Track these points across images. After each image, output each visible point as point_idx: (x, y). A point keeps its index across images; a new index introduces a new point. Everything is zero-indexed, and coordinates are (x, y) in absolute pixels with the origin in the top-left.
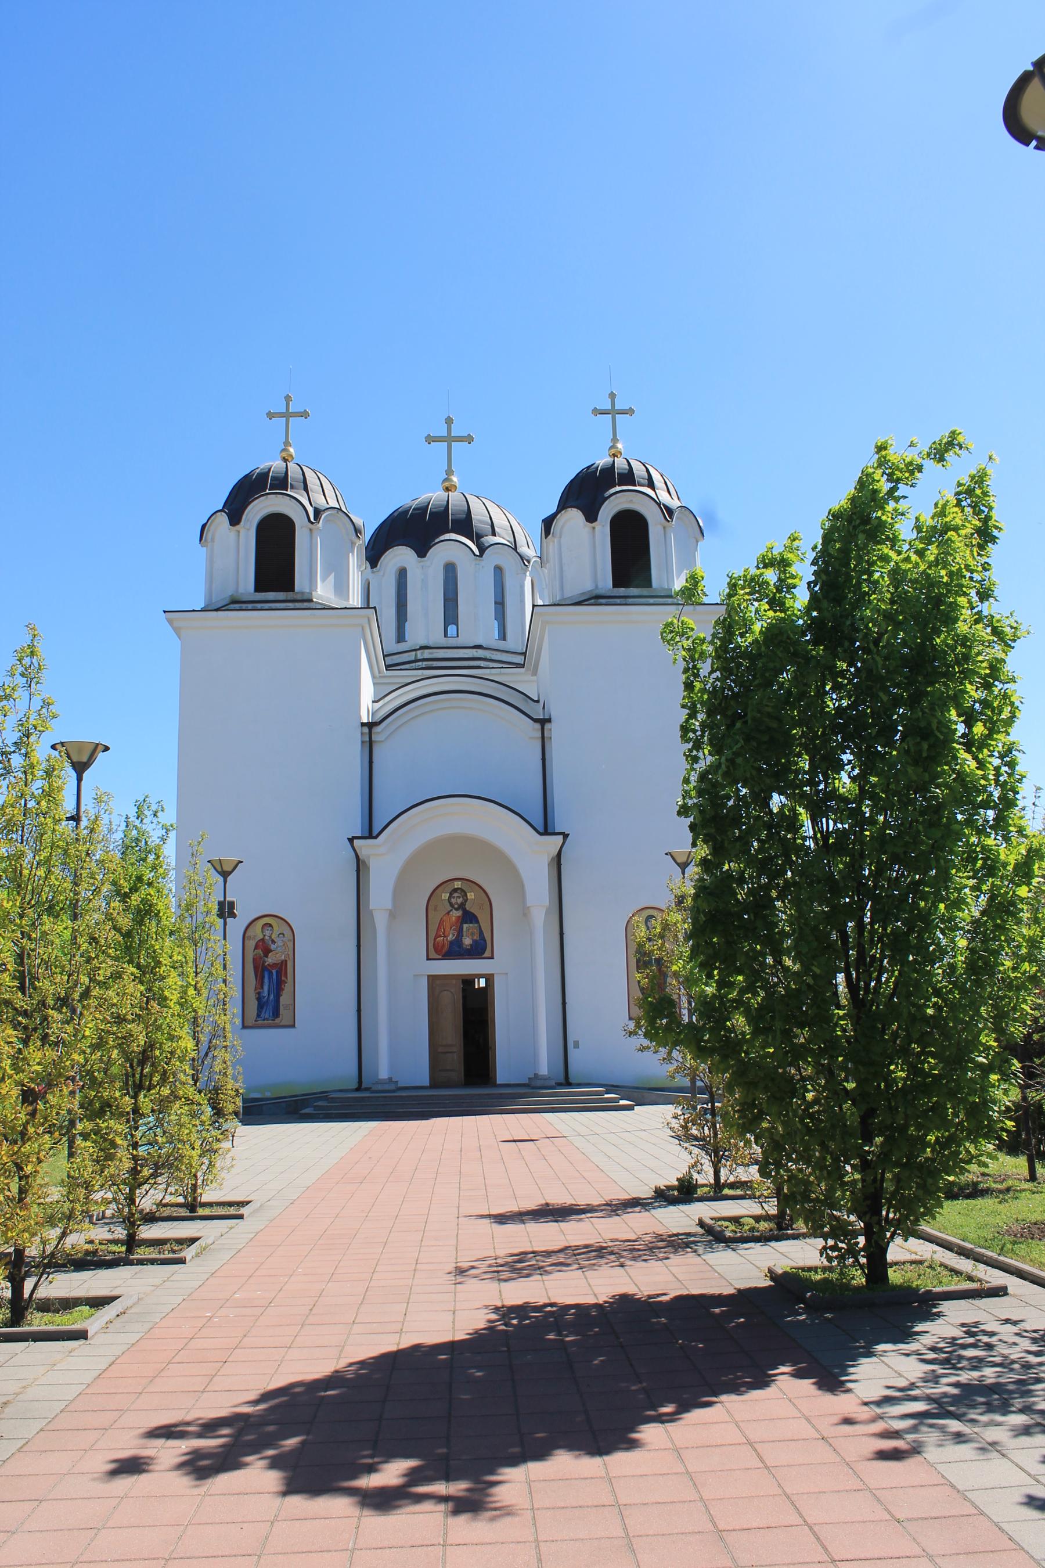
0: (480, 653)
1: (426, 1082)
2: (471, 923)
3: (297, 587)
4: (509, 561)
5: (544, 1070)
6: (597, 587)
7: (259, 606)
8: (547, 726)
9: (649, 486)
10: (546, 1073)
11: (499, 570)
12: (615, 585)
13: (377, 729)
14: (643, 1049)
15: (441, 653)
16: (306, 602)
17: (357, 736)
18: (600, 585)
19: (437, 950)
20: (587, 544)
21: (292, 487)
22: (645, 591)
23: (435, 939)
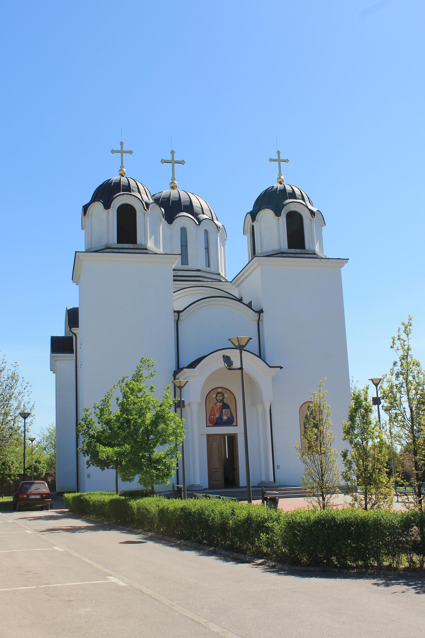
1: (207, 486)
2: (227, 409)
3: (138, 241)
4: (211, 229)
5: (198, 482)
6: (280, 248)
7: (121, 251)
8: (261, 314)
9: (302, 200)
10: (264, 480)
11: (206, 231)
13: (181, 314)
16: (144, 250)
17: (172, 318)
18: (282, 247)
20: (273, 228)
21: (133, 191)
23: (210, 417)
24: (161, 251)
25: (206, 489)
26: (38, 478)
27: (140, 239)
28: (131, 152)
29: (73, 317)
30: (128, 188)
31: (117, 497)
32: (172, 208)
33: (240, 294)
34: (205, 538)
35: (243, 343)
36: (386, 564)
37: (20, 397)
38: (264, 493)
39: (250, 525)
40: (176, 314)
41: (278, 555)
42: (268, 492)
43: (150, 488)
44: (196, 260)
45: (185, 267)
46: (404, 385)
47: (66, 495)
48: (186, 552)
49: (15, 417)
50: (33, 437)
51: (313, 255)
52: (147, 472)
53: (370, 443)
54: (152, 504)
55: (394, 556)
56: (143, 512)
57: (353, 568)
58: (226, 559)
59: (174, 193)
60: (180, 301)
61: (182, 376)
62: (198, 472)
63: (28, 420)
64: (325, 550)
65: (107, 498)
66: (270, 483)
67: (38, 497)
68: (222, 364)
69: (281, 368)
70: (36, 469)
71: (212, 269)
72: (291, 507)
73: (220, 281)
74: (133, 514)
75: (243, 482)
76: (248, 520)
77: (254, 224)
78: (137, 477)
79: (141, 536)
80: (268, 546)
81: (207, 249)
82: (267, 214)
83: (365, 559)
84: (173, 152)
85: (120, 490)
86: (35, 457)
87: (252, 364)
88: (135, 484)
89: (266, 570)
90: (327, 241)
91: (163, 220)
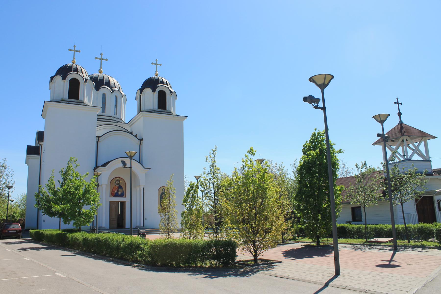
0: (111, 118)
3: (80, 99)
5: (104, 226)
11: (116, 97)
12: (158, 108)
13: (100, 138)
14: (59, 181)
15: (103, 117)
16: (82, 103)
17: (95, 140)
19: (112, 195)
20: (151, 97)
22: (165, 111)
24: (91, 104)
25: (107, 229)
26: (15, 221)
27: (80, 97)
28: (79, 51)
29: (40, 136)
30: (76, 70)
31: (60, 232)
32: (99, 83)
33: (131, 130)
34: (107, 253)
35: (132, 155)
36: (199, 265)
37: (6, 178)
38: (138, 231)
39: (132, 246)
40: (97, 138)
41: (146, 262)
42: (139, 231)
43: (79, 228)
44: (110, 111)
45: (103, 114)
46: (212, 179)
47: (31, 231)
48: (97, 260)
49: (3, 188)
50: (13, 199)
51: (170, 113)
52: (78, 219)
53: (195, 207)
54: (79, 236)
55: (203, 262)
56: (74, 240)
57: (183, 267)
58: (119, 263)
59: (100, 75)
60: (100, 131)
61: (98, 171)
62: (104, 219)
63: (11, 190)
64: (166, 260)
65: (55, 233)
66: (141, 226)
67: (15, 231)
68: (121, 165)
69: (150, 169)
70: (13, 217)
71: (118, 116)
72: (151, 238)
73: (122, 123)
74: (69, 241)
75: (127, 225)
76: (131, 244)
77: (141, 95)
78: (72, 222)
79: (73, 252)
80: (140, 257)
81: (116, 106)
82: (148, 91)
83: (189, 263)
84: (101, 54)
85: (62, 228)
86: (14, 210)
87: (136, 166)
88: (71, 225)
89: (139, 269)
90: (178, 107)
91: (94, 88)
